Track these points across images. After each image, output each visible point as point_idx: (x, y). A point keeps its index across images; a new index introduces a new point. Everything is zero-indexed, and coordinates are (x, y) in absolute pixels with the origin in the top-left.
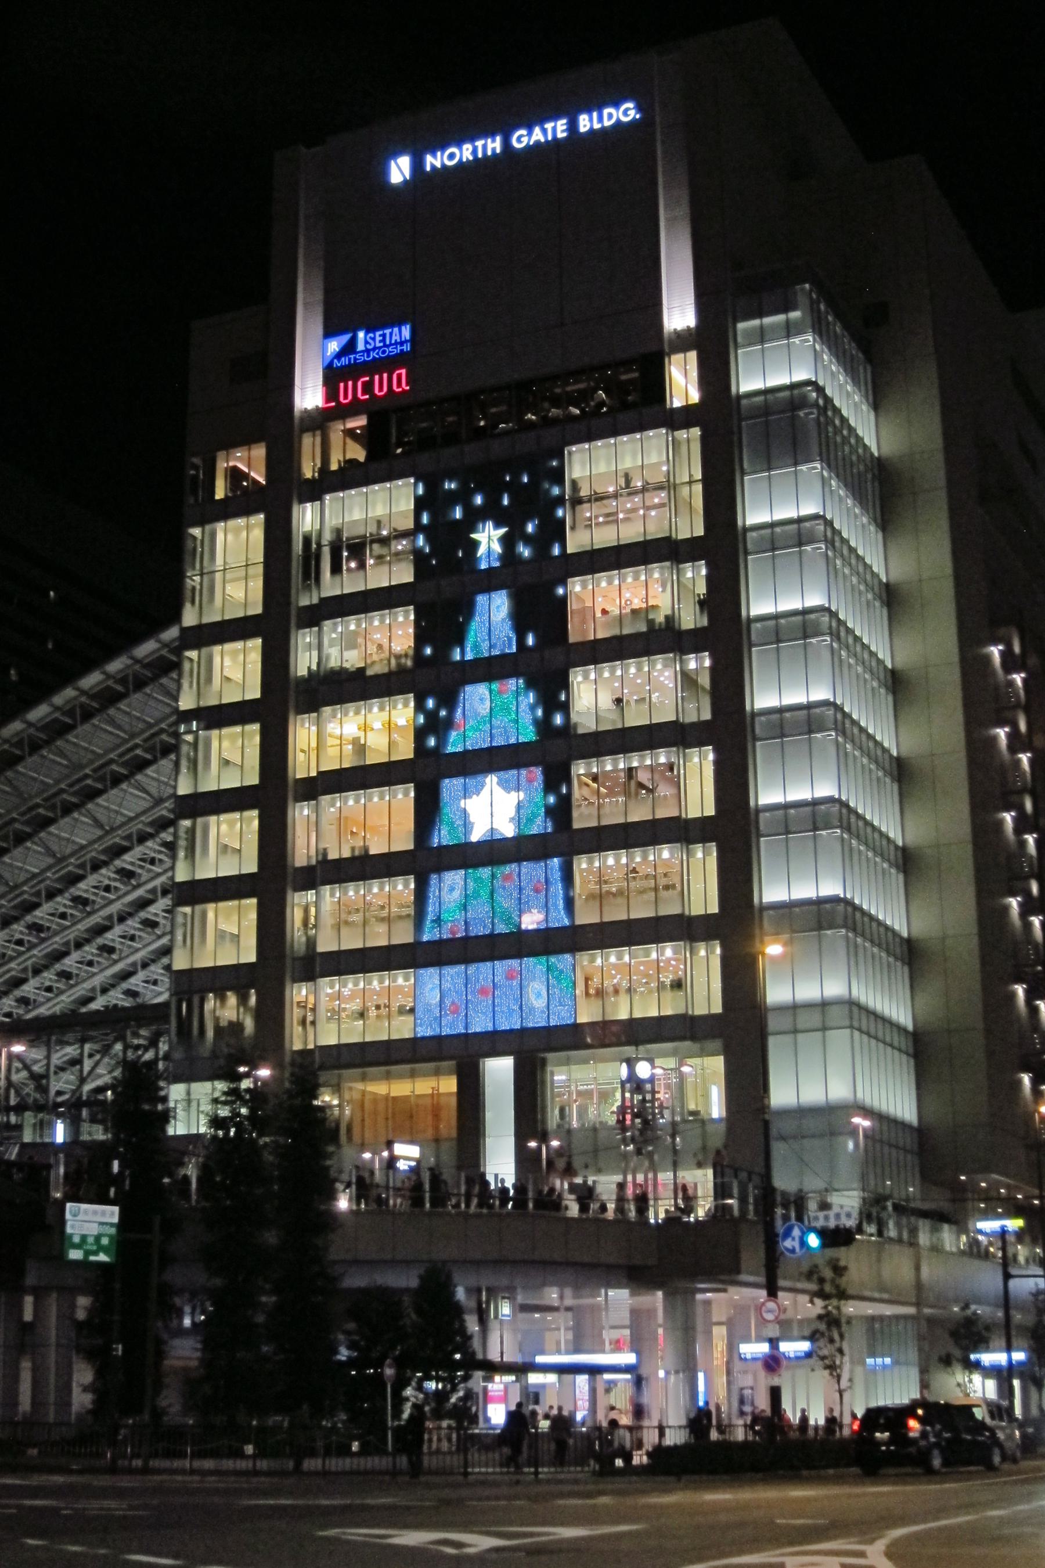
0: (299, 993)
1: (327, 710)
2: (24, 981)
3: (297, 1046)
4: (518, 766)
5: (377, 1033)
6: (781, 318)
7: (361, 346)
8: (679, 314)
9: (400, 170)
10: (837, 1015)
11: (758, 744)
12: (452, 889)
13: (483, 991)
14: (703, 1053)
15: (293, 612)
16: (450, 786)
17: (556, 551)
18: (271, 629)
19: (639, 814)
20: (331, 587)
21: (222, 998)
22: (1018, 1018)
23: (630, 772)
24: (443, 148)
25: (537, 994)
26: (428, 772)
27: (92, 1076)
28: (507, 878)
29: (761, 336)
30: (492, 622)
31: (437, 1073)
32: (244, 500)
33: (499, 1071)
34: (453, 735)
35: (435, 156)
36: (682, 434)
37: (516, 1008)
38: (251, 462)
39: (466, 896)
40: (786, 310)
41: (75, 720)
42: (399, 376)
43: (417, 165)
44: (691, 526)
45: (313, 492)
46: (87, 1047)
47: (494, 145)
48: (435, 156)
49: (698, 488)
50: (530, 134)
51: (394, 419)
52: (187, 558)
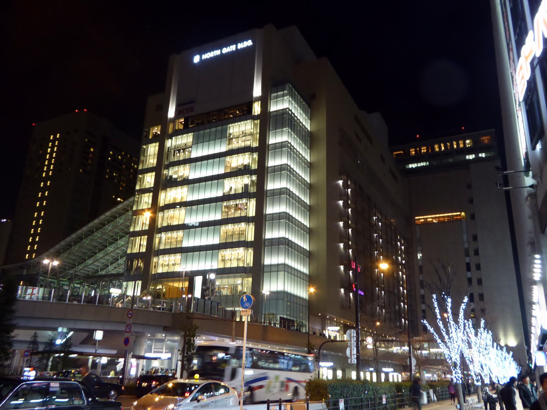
0: (155, 260)
1: (168, 189)
3: (153, 273)
6: (282, 93)
8: (257, 91)
9: (196, 59)
10: (281, 268)
11: (268, 198)
14: (248, 277)
15: (163, 165)
18: (157, 170)
19: (238, 214)
20: (173, 159)
22: (341, 273)
23: (237, 205)
29: (277, 97)
32: (157, 138)
36: (256, 121)
38: (156, 130)
44: (255, 144)
49: (258, 135)
51: (190, 118)
52: (142, 153)
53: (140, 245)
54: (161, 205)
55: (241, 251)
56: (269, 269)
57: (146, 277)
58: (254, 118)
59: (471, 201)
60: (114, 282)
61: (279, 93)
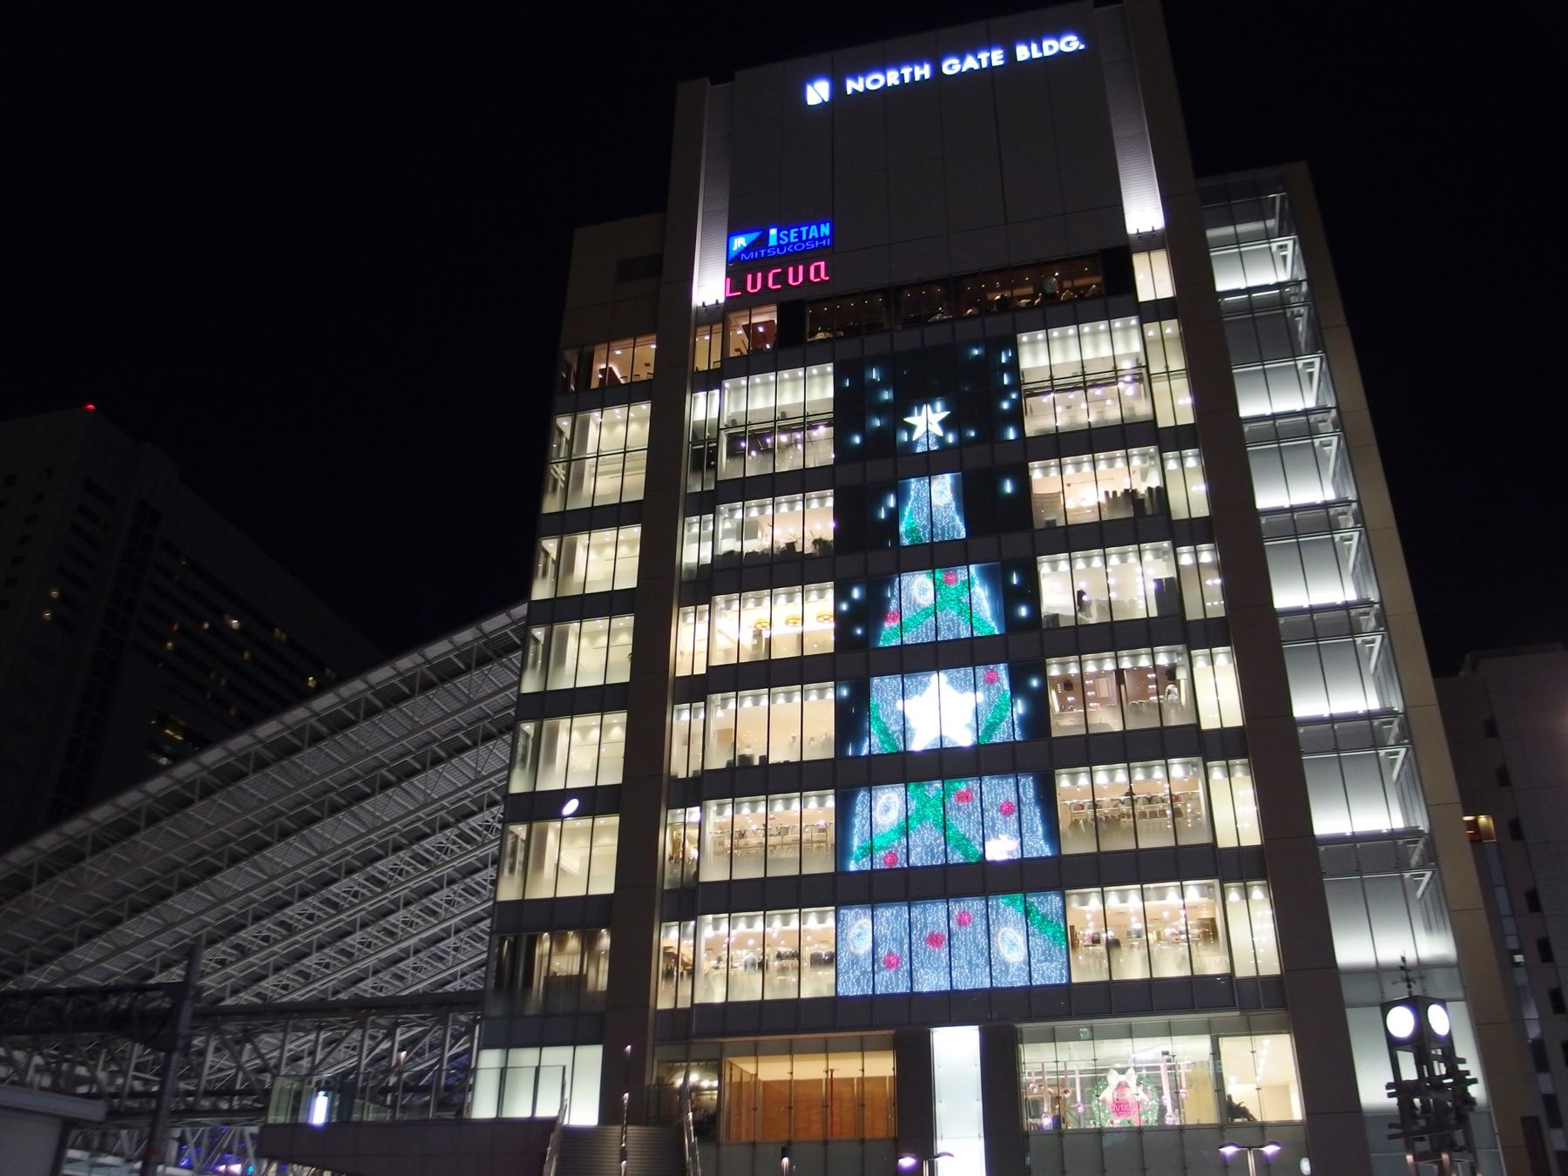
0: (670, 937)
1: (720, 599)
2: (264, 977)
4: (973, 662)
5: (781, 988)
7: (773, 241)
8: (1143, 211)
12: (887, 809)
13: (934, 940)
16: (883, 688)
17: (1011, 434)
18: (656, 515)
21: (559, 942)
24: (865, 74)
25: (1011, 947)
26: (858, 662)
27: (325, 1065)
28: (964, 797)
30: (935, 503)
31: (862, 1048)
33: (956, 1051)
34: (889, 626)
35: (856, 80)
37: (982, 961)
38: (627, 359)
39: (907, 817)
40: (1263, 218)
41: (357, 715)
42: (817, 269)
43: (837, 89)
45: (711, 381)
46: (323, 1036)
47: (924, 71)
48: (856, 80)
50: (962, 62)
53: (580, 860)
54: (683, 670)
55: (1180, 902)
56: (1370, 991)
57: (628, 1025)
58: (1156, 311)
59: (1503, 778)
60: (123, 1045)
61: (1243, 228)
